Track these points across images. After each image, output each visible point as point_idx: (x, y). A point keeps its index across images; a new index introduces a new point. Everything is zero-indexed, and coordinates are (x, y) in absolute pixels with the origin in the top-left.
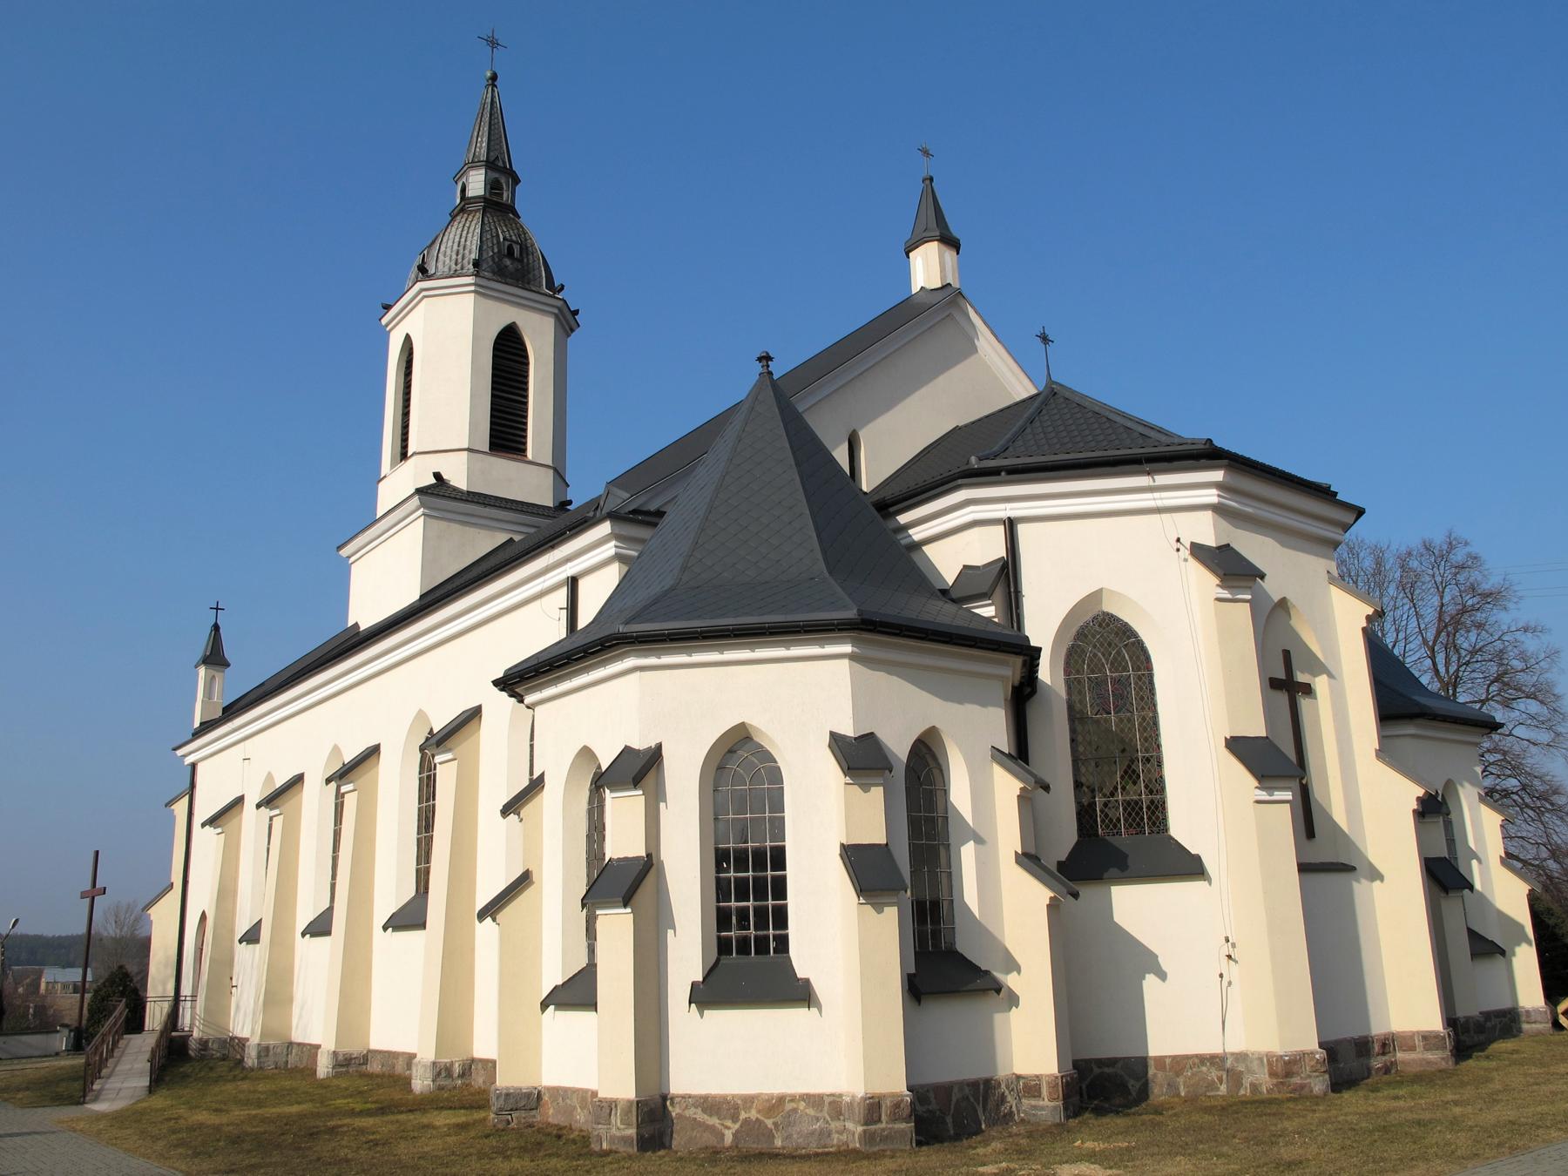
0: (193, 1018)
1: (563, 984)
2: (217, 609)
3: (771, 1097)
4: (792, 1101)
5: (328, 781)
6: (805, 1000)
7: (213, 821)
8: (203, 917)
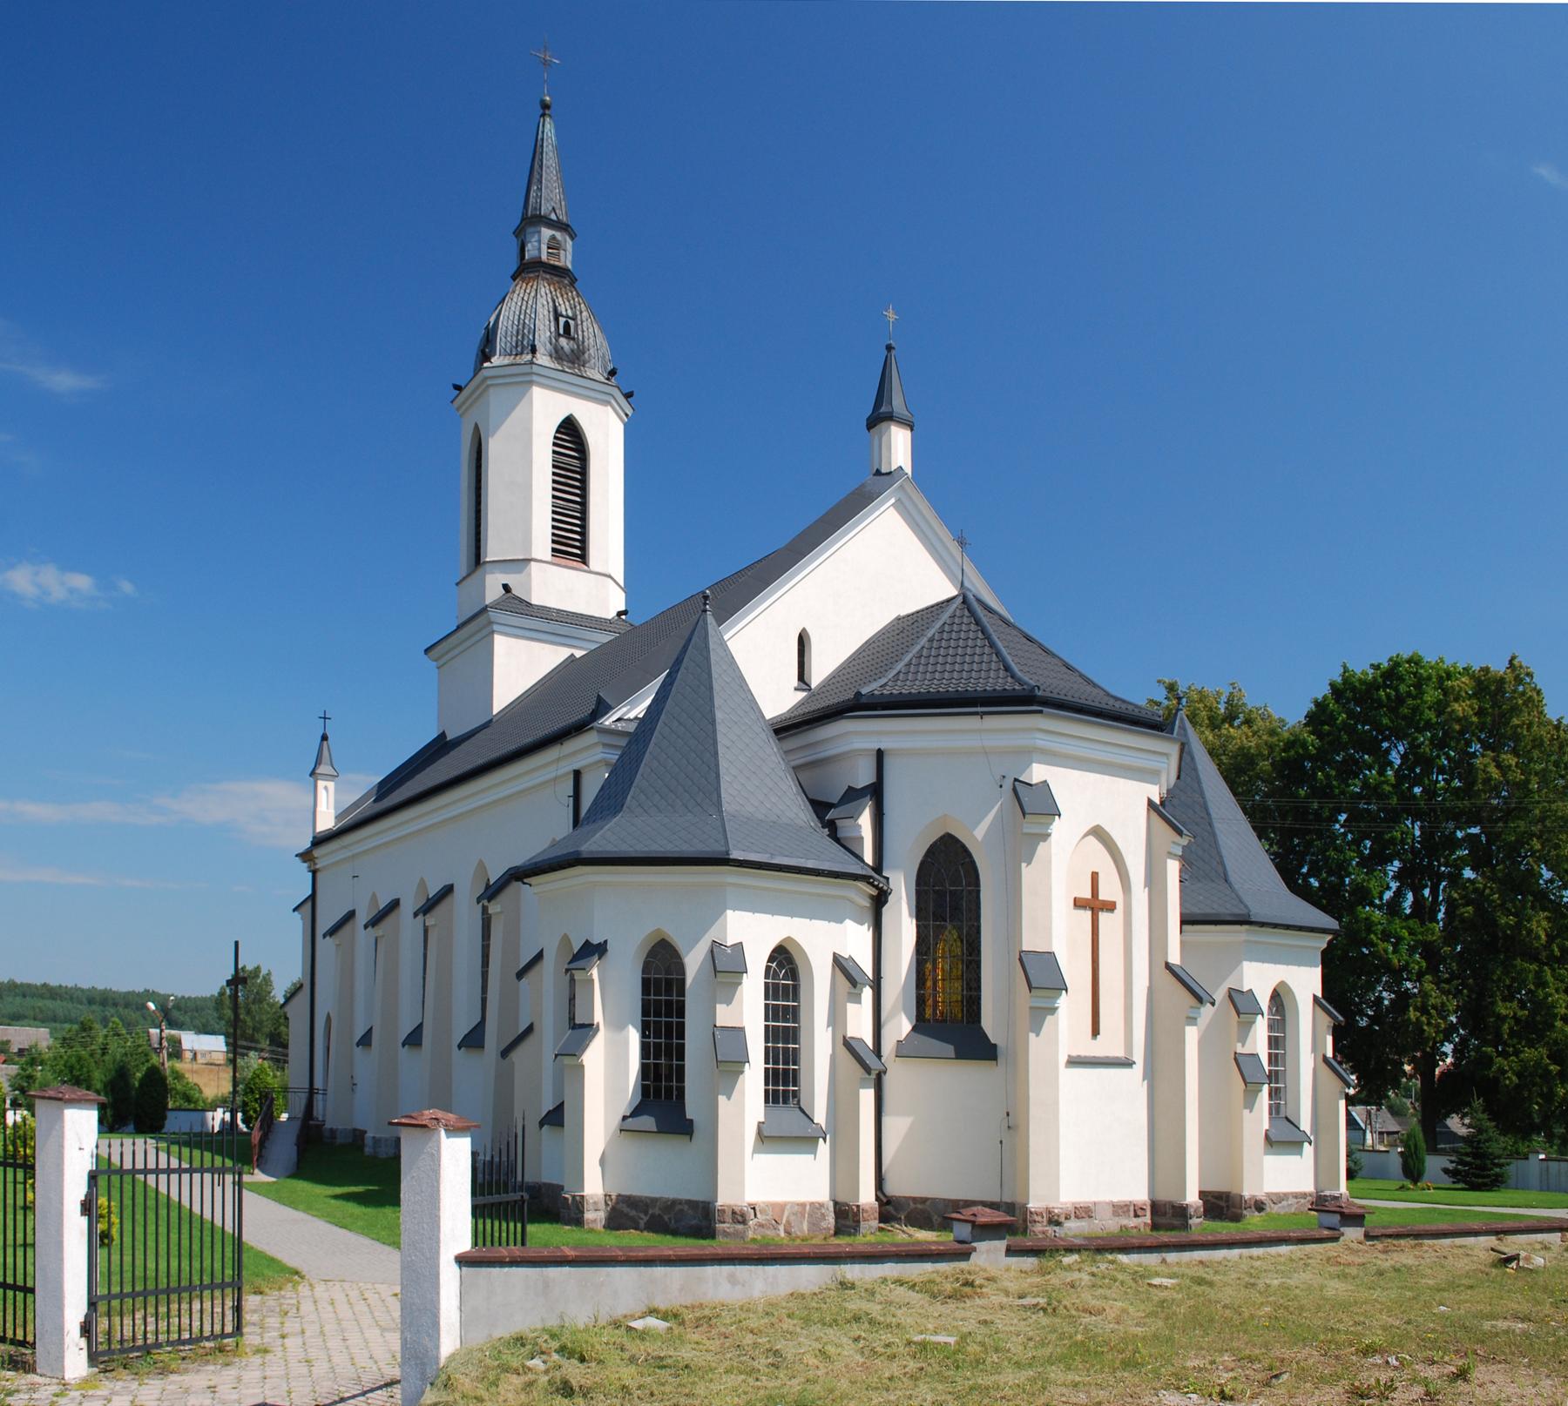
0: (324, 1109)
1: (554, 1109)
2: (325, 718)
3: (668, 1200)
4: (680, 1203)
5: (416, 915)
6: (687, 1134)
7: (332, 932)
8: (329, 1018)
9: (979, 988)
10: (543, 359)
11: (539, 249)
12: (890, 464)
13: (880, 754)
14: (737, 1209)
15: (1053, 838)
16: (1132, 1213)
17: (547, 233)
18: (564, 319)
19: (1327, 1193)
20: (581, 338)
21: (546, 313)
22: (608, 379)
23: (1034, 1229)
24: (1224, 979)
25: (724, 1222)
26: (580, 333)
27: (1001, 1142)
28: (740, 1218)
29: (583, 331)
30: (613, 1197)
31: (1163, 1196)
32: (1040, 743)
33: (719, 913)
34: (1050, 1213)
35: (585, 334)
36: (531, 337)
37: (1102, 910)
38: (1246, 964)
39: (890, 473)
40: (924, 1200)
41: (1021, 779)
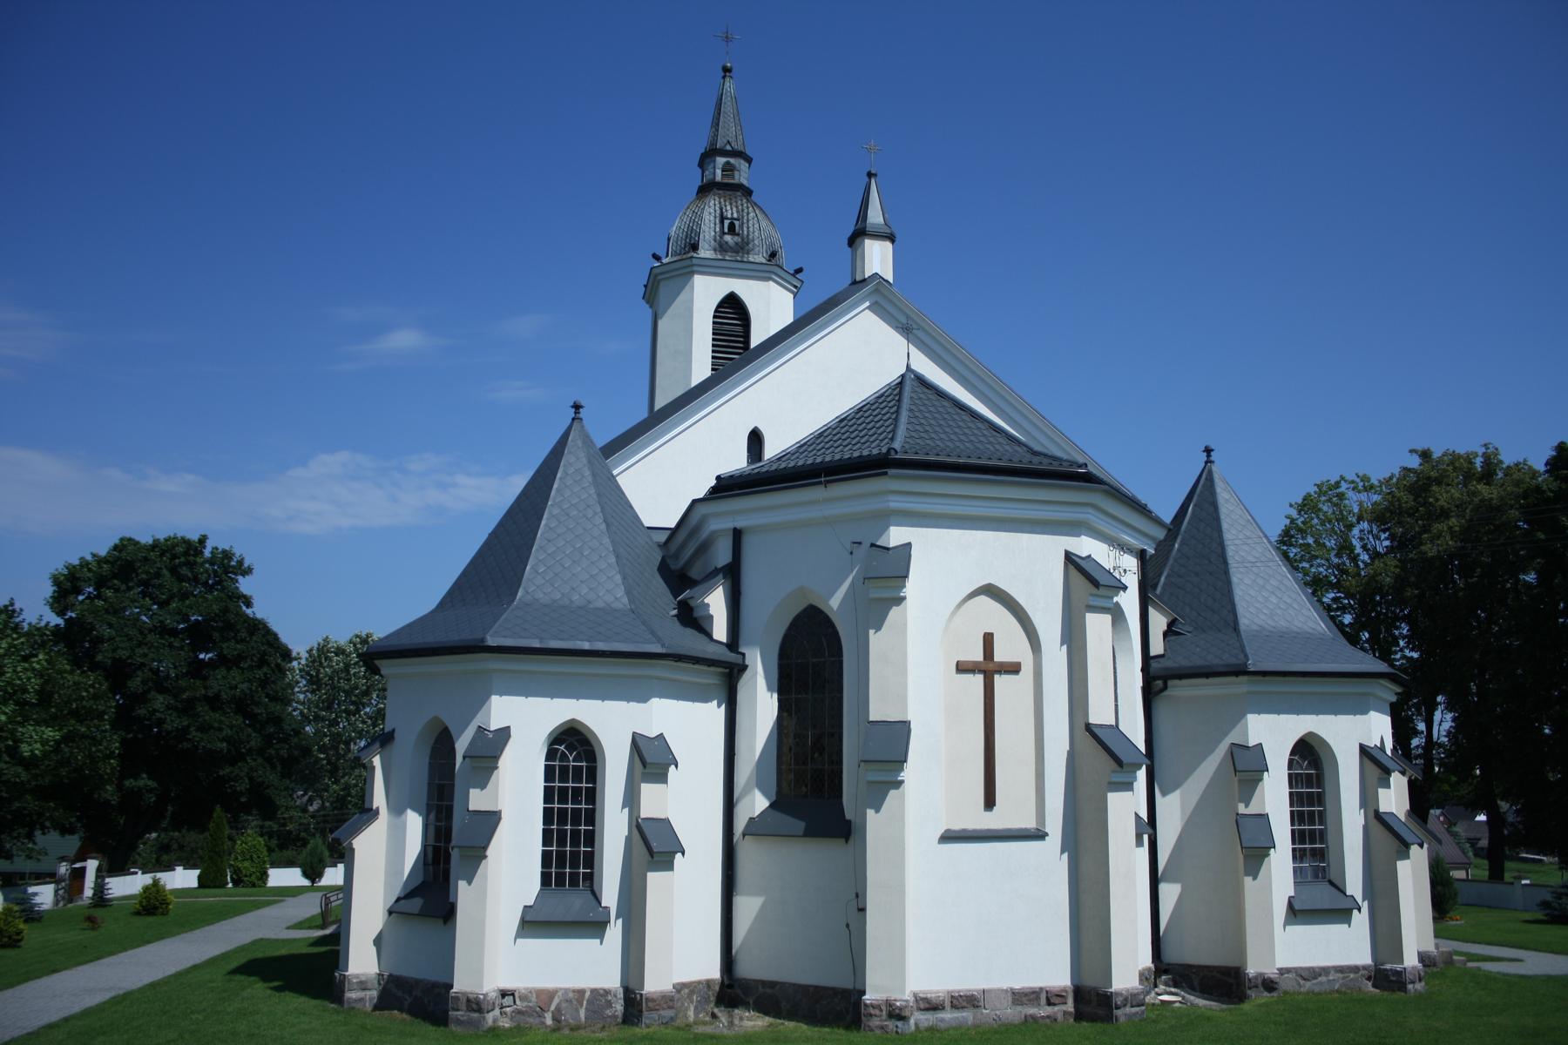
9: (840, 762)
10: (705, 252)
11: (714, 173)
12: (864, 272)
13: (737, 534)
14: (471, 996)
15: (909, 602)
16: (1043, 1000)
17: (721, 161)
18: (729, 221)
19: (1388, 966)
20: (745, 233)
21: (712, 218)
22: (769, 261)
23: (871, 1024)
24: (1225, 734)
25: (458, 1010)
26: (745, 229)
27: (848, 926)
28: (474, 1006)
29: (748, 228)
30: (385, 977)
31: (1089, 981)
32: (893, 505)
33: (484, 699)
34: (890, 1006)
35: (751, 229)
36: (697, 239)
37: (999, 672)
38: (1250, 717)
39: (864, 280)
40: (772, 984)
41: (878, 543)
